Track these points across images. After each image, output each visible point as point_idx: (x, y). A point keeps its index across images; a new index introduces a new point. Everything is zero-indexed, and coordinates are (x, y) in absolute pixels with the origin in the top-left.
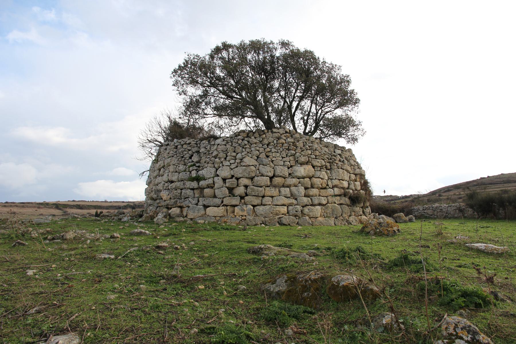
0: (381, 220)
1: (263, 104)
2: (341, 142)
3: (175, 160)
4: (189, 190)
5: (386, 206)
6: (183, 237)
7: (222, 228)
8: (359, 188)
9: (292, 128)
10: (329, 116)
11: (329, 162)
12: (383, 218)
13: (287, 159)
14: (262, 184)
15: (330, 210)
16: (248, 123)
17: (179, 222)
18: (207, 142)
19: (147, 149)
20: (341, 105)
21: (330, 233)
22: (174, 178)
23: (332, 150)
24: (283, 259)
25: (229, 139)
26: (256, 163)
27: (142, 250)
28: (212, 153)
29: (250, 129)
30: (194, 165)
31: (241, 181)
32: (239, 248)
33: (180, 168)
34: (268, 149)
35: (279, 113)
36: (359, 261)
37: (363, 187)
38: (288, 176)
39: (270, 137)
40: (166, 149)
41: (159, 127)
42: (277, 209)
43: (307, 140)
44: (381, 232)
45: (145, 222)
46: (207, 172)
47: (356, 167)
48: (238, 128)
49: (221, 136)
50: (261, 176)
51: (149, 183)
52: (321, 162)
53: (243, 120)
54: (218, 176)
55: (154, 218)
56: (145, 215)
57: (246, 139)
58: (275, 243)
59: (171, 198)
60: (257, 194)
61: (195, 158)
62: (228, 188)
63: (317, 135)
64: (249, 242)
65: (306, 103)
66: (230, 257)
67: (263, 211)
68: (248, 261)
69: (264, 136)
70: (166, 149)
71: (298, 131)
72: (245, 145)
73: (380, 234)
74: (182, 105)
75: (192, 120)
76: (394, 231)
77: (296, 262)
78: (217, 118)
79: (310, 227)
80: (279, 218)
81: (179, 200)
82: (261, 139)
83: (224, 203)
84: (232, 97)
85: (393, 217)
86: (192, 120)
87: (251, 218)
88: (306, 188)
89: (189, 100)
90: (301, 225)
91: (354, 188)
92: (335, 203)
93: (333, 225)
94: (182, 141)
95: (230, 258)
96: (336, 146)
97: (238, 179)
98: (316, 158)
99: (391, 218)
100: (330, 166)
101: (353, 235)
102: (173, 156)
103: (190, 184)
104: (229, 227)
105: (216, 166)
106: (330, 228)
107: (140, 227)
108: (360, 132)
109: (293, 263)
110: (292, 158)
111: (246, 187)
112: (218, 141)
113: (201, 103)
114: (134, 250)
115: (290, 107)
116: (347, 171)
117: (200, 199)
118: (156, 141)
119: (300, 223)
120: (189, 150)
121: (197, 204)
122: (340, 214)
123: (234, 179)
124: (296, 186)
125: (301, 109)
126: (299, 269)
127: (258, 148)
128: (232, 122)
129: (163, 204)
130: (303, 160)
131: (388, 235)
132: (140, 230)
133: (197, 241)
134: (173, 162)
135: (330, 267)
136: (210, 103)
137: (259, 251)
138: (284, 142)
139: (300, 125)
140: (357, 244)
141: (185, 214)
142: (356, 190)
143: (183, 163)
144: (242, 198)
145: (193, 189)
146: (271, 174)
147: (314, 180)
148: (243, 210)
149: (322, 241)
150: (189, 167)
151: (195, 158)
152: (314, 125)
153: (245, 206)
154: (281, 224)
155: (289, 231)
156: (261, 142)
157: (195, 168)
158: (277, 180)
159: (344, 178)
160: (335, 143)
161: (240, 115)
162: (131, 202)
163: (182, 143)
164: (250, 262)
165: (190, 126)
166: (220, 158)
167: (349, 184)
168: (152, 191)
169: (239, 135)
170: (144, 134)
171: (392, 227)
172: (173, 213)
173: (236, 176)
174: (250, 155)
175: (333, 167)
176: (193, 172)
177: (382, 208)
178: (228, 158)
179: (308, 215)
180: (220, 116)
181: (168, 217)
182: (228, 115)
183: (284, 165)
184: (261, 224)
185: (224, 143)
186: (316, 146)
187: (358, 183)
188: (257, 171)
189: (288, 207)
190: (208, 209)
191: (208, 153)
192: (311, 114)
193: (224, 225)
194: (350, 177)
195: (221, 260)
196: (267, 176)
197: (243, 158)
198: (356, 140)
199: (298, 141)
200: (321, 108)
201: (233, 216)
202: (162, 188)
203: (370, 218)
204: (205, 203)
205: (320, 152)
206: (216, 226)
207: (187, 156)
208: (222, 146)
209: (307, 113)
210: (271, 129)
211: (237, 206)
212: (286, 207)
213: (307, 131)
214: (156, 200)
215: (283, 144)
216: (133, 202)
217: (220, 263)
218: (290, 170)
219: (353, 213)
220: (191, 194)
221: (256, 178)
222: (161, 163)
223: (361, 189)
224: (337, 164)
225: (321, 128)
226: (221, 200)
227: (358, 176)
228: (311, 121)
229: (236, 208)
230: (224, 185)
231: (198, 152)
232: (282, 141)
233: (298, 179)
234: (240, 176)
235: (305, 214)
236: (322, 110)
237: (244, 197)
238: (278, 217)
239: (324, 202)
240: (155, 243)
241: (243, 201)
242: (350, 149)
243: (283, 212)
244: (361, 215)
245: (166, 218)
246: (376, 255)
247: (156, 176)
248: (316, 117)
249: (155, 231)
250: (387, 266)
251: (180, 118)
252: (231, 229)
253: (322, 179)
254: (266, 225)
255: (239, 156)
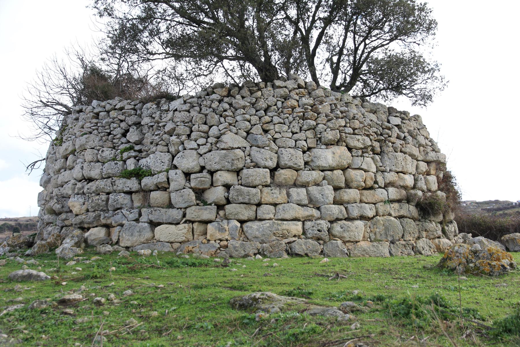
0: (478, 247)
1: (257, 33)
2: (401, 103)
3: (94, 140)
4: (123, 195)
5: (488, 220)
6: (111, 280)
7: (183, 263)
8: (434, 187)
9: (309, 79)
10: (379, 55)
11: (379, 141)
12: (480, 242)
13: (301, 135)
14: (257, 182)
15: (382, 228)
16: (228, 71)
17: (105, 254)
18: (155, 106)
19: (41, 119)
20: (401, 32)
21: (381, 270)
22: (94, 173)
23: (384, 117)
24: (295, 318)
25: (195, 100)
26: (245, 144)
27: (32, 308)
28: (164, 126)
29: (232, 82)
30: (131, 148)
31: (217, 176)
32: (216, 299)
33: (104, 154)
34: (267, 119)
35: (285, 49)
36: (435, 322)
37: (443, 185)
38: (302, 166)
39: (269, 96)
40: (77, 119)
41: (62, 77)
42: (284, 227)
43: (337, 99)
44: (478, 269)
45: (39, 256)
46: (156, 160)
47: (429, 149)
48: (212, 81)
49: (181, 95)
50: (254, 167)
51: (45, 183)
52: (364, 140)
53: (219, 64)
54: (176, 167)
55: (57, 247)
56: (38, 242)
57: (226, 99)
58: (280, 289)
59: (88, 211)
60: (246, 201)
61: (133, 136)
62: (194, 189)
63: (357, 89)
64: (233, 288)
65: (336, 31)
66: (199, 316)
67: (258, 230)
68: (231, 323)
69: (259, 93)
70: (77, 119)
71: (322, 83)
72: (225, 111)
73: (476, 272)
74: (105, 36)
75: (125, 65)
76: (503, 266)
77: (320, 324)
78: (172, 61)
79: (344, 260)
80: (289, 243)
81: (104, 214)
82: (254, 100)
83: (188, 217)
84: (199, 23)
85: (501, 242)
86: (125, 65)
87: (237, 243)
88: (336, 189)
89: (117, 27)
90: (328, 256)
91: (425, 188)
92: (390, 215)
93: (388, 255)
94: (107, 104)
95: (199, 319)
96: (391, 111)
97: (212, 173)
98: (354, 134)
99: (496, 243)
100: (381, 147)
101: (425, 274)
102: (91, 133)
103: (125, 183)
104: (197, 262)
105: (172, 149)
106: (381, 260)
107: (27, 265)
108: (437, 84)
109: (314, 325)
110: (310, 134)
111: (227, 187)
112: (175, 104)
113: (142, 31)
114: (16, 310)
115: (306, 39)
116: (412, 156)
117: (144, 210)
118: (58, 104)
119: (326, 251)
120: (122, 121)
121: (137, 220)
122: (401, 235)
123: (205, 173)
124: (318, 185)
125: (326, 42)
126: (324, 337)
127: (247, 116)
128: (201, 69)
129: (73, 220)
130: (330, 137)
131: (490, 275)
132: (27, 271)
133: (138, 289)
134: (91, 144)
135: (382, 333)
136: (158, 32)
137: (251, 305)
138: (296, 104)
139: (324, 72)
140: (432, 290)
141: (114, 239)
142: (429, 190)
143: (110, 144)
144: (220, 207)
145: (130, 193)
146: (272, 164)
147: (352, 173)
148: (222, 230)
149: (366, 284)
150: (122, 153)
151: (133, 136)
152: (351, 72)
153: (225, 221)
154: (291, 253)
155: (306, 267)
156: (253, 104)
157: (133, 153)
158: (283, 175)
159: (405, 168)
160: (388, 104)
161: (215, 56)
162: (11, 220)
163: (108, 107)
164: (235, 325)
165: (121, 76)
166: (178, 135)
167: (416, 180)
168: (51, 198)
169: (214, 93)
170: (33, 91)
171: (498, 259)
172: (92, 237)
173: (208, 167)
174: (234, 129)
175: (385, 149)
176: (128, 162)
177: (480, 225)
178: (194, 135)
179: (341, 238)
180: (178, 57)
181: (83, 245)
182: (193, 55)
183: (296, 147)
184: (255, 254)
185: (187, 107)
186: (354, 110)
187: (432, 179)
188: (247, 158)
189: (303, 222)
190: (158, 229)
191: (156, 125)
192: (345, 52)
193: (187, 257)
194: (417, 168)
195: (181, 322)
196: (265, 167)
197: (221, 134)
198: (430, 97)
199: (321, 103)
200: (364, 40)
201: (205, 241)
202: (70, 192)
203: (456, 242)
204: (153, 218)
205: (361, 123)
206: (173, 259)
207: (118, 132)
208: (182, 113)
209: (338, 49)
210: (272, 81)
211: (210, 222)
212: (300, 224)
213: (338, 84)
214: (60, 213)
215: (293, 108)
216: (16, 220)
217: (180, 329)
218: (306, 155)
219: (424, 234)
220: (126, 202)
221: (245, 171)
222: (67, 146)
223: (439, 189)
224: (393, 143)
225: (365, 78)
226: (181, 212)
227: (433, 165)
228: (344, 65)
229: (209, 226)
230: (188, 184)
231: (138, 124)
232: (292, 102)
233: (322, 171)
234: (217, 167)
235: (335, 236)
236: (365, 45)
237: (224, 205)
238: (287, 241)
239: (370, 213)
240: (57, 295)
241: (221, 213)
242: (418, 116)
243: (294, 232)
244: (439, 237)
245: (79, 246)
246: (469, 311)
247: (60, 170)
248: (355, 57)
249: (57, 271)
250: (491, 332)
251: (103, 59)
252: (201, 265)
253: (365, 171)
254: (264, 256)
255: (214, 131)
